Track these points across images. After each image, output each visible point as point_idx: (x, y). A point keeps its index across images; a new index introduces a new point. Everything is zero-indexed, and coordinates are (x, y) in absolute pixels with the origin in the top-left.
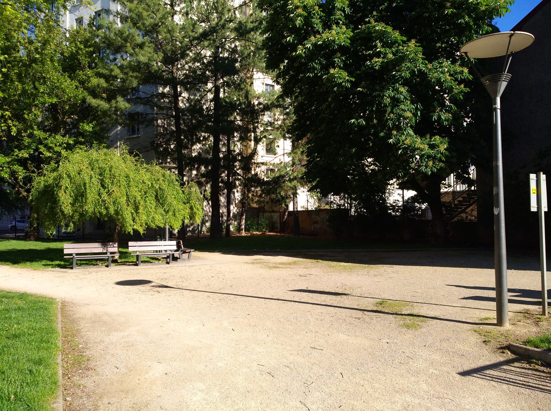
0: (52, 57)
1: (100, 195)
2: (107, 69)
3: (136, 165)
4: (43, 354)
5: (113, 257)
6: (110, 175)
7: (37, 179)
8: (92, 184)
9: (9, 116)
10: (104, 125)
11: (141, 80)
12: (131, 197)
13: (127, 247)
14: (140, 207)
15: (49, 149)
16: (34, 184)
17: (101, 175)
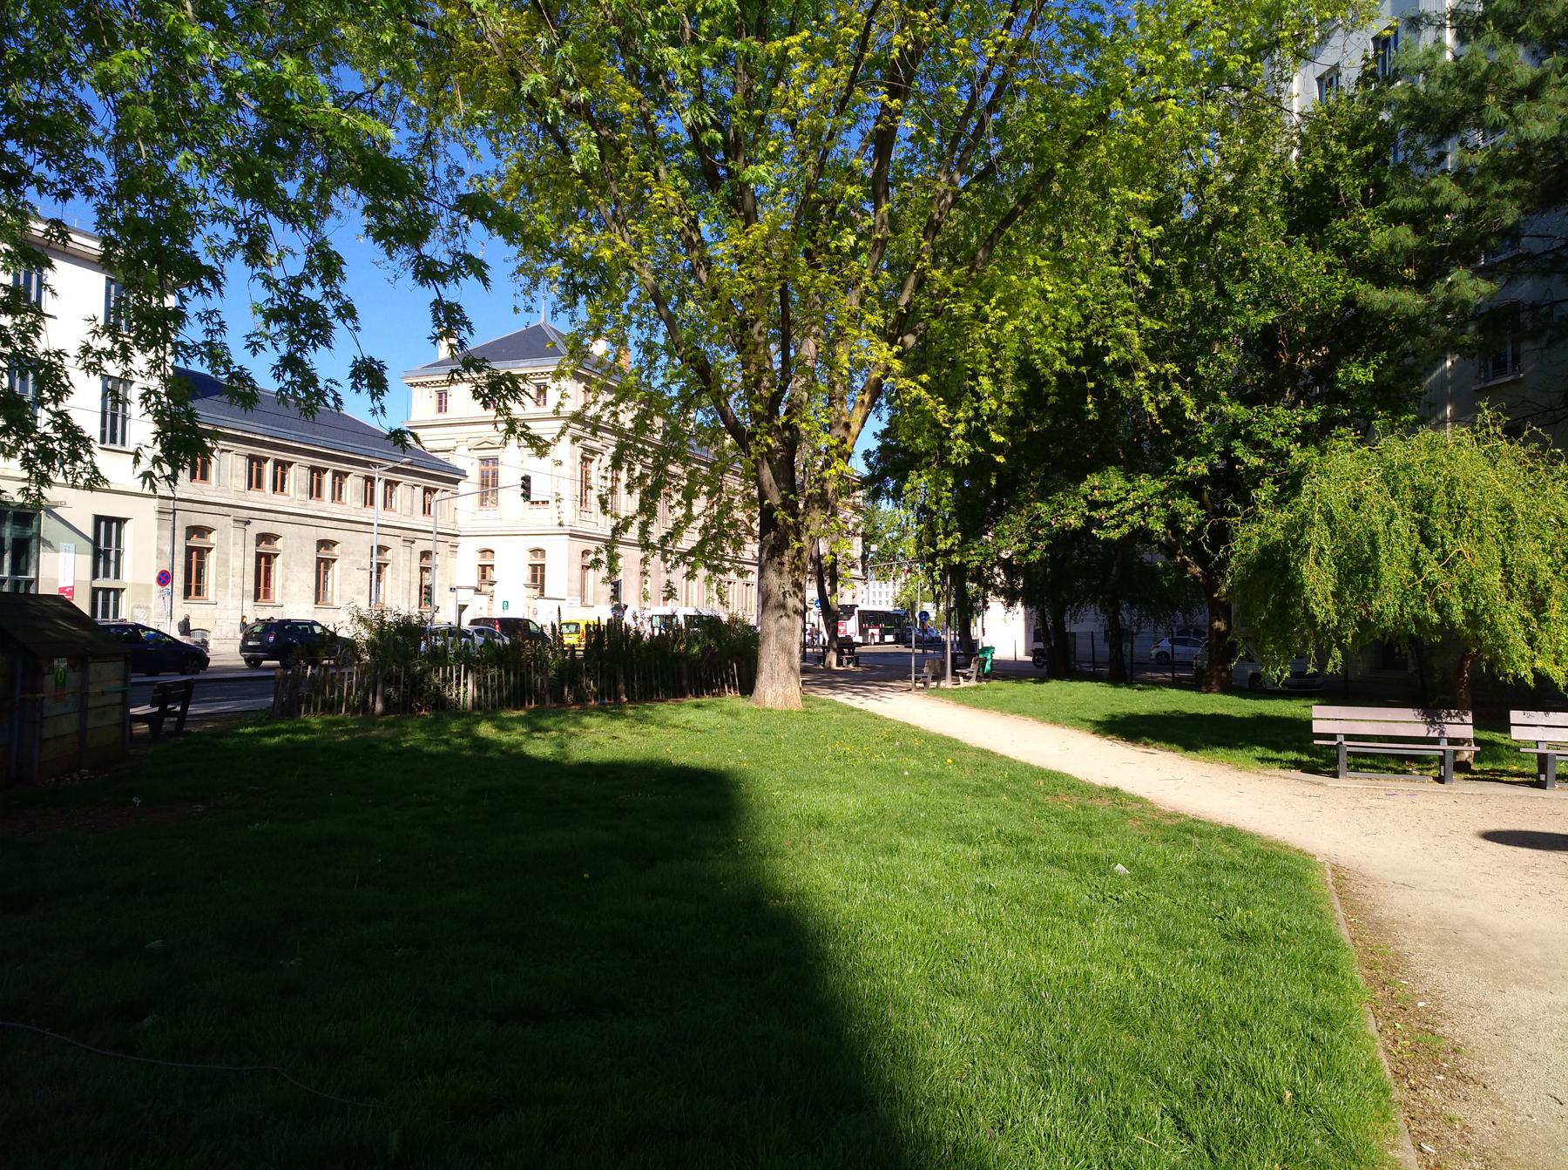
0: (1262, 200)
1: (1416, 566)
2: (1418, 194)
3: (1531, 470)
4: (1325, 1000)
5: (1456, 753)
6: (1449, 505)
7: (1243, 532)
8: (1394, 536)
9: (1174, 373)
10: (1409, 361)
11: (1530, 200)
12: (1517, 571)
13: (1505, 727)
14: (1552, 601)
15: (1256, 445)
16: (1237, 545)
17: (1418, 507)
